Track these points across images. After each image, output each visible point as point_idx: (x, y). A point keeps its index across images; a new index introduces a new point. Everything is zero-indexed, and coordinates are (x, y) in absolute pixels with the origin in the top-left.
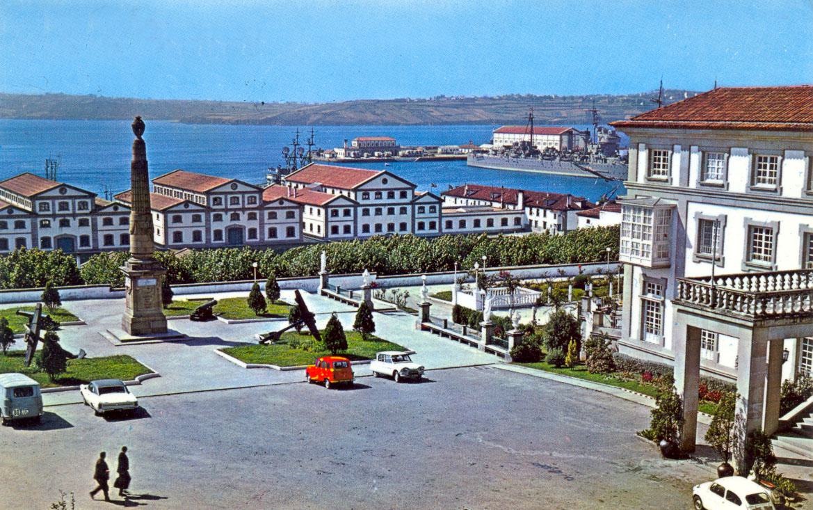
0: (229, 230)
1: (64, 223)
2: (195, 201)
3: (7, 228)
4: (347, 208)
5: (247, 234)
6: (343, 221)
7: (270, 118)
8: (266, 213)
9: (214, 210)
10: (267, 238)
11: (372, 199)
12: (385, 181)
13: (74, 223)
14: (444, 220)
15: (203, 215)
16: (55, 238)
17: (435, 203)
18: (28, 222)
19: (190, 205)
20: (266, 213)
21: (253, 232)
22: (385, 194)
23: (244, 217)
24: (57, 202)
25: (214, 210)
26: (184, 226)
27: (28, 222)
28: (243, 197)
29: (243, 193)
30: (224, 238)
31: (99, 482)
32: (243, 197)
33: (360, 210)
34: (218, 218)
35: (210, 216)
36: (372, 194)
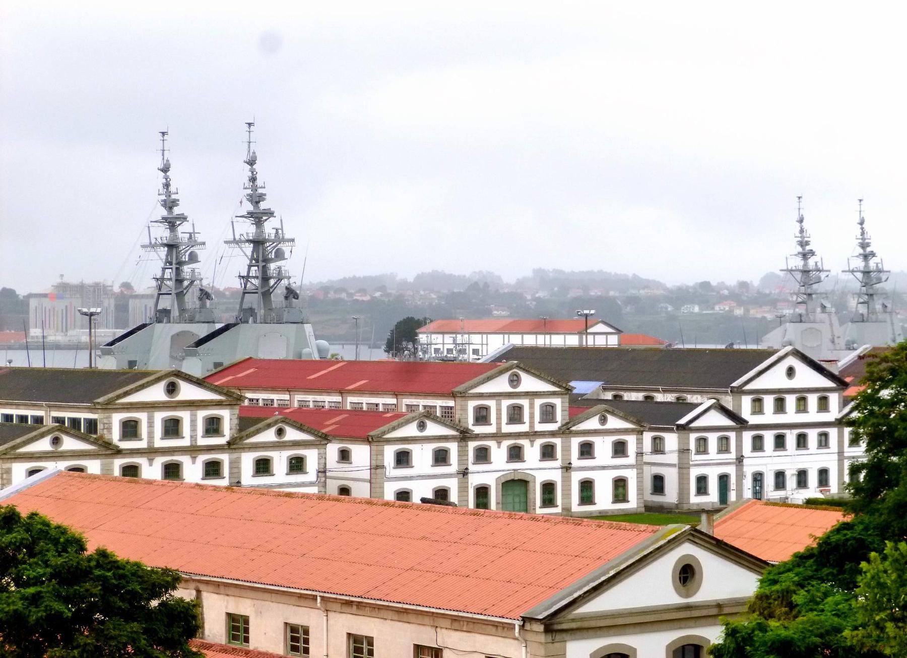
3: (628, 502)
7: (327, 341)
8: (575, 442)
9: (477, 437)
10: (576, 507)
14: (454, 465)
15: (453, 448)
21: (548, 488)
23: (532, 451)
25: (477, 437)
28: (532, 406)
32: (532, 406)
33: (748, 436)
36: (769, 402)
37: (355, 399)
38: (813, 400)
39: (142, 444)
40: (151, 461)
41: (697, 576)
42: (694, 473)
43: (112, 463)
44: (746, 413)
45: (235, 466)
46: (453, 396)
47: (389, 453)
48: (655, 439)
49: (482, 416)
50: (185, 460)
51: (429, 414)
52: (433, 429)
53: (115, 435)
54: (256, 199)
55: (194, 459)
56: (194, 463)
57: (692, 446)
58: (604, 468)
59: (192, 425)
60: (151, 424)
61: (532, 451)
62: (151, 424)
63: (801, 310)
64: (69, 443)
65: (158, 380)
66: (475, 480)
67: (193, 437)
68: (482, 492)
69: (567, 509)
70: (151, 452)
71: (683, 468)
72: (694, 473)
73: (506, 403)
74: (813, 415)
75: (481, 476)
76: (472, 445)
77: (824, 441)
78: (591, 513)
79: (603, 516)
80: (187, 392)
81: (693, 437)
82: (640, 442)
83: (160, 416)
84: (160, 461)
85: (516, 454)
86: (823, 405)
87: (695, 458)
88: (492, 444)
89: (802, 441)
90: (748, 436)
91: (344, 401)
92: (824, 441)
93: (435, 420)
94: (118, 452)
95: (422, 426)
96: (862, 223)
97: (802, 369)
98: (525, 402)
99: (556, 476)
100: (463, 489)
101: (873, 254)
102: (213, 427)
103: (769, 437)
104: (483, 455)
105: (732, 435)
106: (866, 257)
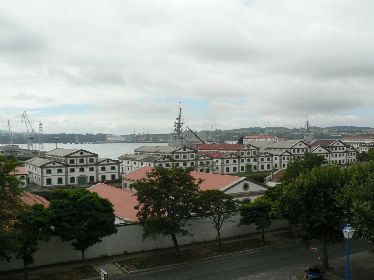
0: (86, 177)
1: (82, 170)
2: (57, 161)
4: (208, 161)
5: (253, 168)
6: (110, 173)
11: (334, 151)
12: (300, 145)
13: (87, 169)
15: (237, 160)
16: (77, 177)
17: (235, 158)
18: (64, 169)
19: (266, 154)
20: (260, 158)
21: (255, 167)
22: (338, 148)
23: (252, 160)
24: (79, 159)
26: (107, 172)
27: (64, 169)
28: (252, 152)
29: (87, 157)
30: (245, 170)
31: (318, 226)
33: (274, 157)
34: (72, 170)
35: (68, 170)
36: (296, 150)
37: (203, 150)
38: (342, 148)
39: (179, 159)
40: (181, 163)
41: (248, 187)
42: (282, 163)
43: (68, 168)
44: (292, 152)
45: (196, 163)
46: (237, 150)
47: (225, 160)
48: (275, 157)
49: (242, 154)
50: (187, 162)
51: (233, 154)
52: (233, 156)
53: (69, 162)
54: (180, 116)
55: (189, 162)
56: (87, 168)
57: (282, 159)
58: (231, 165)
59: (188, 156)
60: (181, 156)
61: (252, 160)
62: (181, 156)
63: (307, 134)
64: (166, 160)
65: (246, 146)
66: (241, 165)
67: (189, 158)
68: (243, 168)
69: (259, 170)
70: (181, 161)
71: (281, 162)
72: (282, 163)
73: (247, 151)
74: (342, 150)
75: (242, 165)
76: (241, 159)
77: (344, 155)
78: (61, 186)
79: (232, 174)
80: (187, 150)
81: (282, 157)
82: (272, 158)
83: (182, 155)
84: (182, 163)
85: (249, 161)
86: (343, 149)
87: (283, 161)
88: (244, 159)
89: (340, 155)
90: (331, 154)
91: (218, 151)
92: (344, 155)
93: (234, 155)
94: (69, 166)
95: (231, 156)
96: (307, 119)
97: (339, 143)
98: (250, 151)
99: (256, 164)
100: (239, 167)
101: (309, 124)
102: (192, 156)
103: (334, 155)
104: (243, 161)
105: (290, 157)
106: (308, 125)
